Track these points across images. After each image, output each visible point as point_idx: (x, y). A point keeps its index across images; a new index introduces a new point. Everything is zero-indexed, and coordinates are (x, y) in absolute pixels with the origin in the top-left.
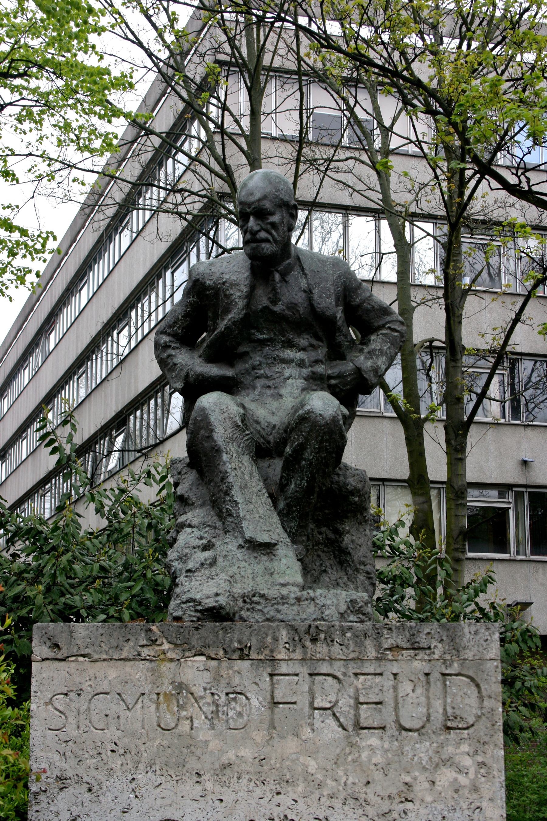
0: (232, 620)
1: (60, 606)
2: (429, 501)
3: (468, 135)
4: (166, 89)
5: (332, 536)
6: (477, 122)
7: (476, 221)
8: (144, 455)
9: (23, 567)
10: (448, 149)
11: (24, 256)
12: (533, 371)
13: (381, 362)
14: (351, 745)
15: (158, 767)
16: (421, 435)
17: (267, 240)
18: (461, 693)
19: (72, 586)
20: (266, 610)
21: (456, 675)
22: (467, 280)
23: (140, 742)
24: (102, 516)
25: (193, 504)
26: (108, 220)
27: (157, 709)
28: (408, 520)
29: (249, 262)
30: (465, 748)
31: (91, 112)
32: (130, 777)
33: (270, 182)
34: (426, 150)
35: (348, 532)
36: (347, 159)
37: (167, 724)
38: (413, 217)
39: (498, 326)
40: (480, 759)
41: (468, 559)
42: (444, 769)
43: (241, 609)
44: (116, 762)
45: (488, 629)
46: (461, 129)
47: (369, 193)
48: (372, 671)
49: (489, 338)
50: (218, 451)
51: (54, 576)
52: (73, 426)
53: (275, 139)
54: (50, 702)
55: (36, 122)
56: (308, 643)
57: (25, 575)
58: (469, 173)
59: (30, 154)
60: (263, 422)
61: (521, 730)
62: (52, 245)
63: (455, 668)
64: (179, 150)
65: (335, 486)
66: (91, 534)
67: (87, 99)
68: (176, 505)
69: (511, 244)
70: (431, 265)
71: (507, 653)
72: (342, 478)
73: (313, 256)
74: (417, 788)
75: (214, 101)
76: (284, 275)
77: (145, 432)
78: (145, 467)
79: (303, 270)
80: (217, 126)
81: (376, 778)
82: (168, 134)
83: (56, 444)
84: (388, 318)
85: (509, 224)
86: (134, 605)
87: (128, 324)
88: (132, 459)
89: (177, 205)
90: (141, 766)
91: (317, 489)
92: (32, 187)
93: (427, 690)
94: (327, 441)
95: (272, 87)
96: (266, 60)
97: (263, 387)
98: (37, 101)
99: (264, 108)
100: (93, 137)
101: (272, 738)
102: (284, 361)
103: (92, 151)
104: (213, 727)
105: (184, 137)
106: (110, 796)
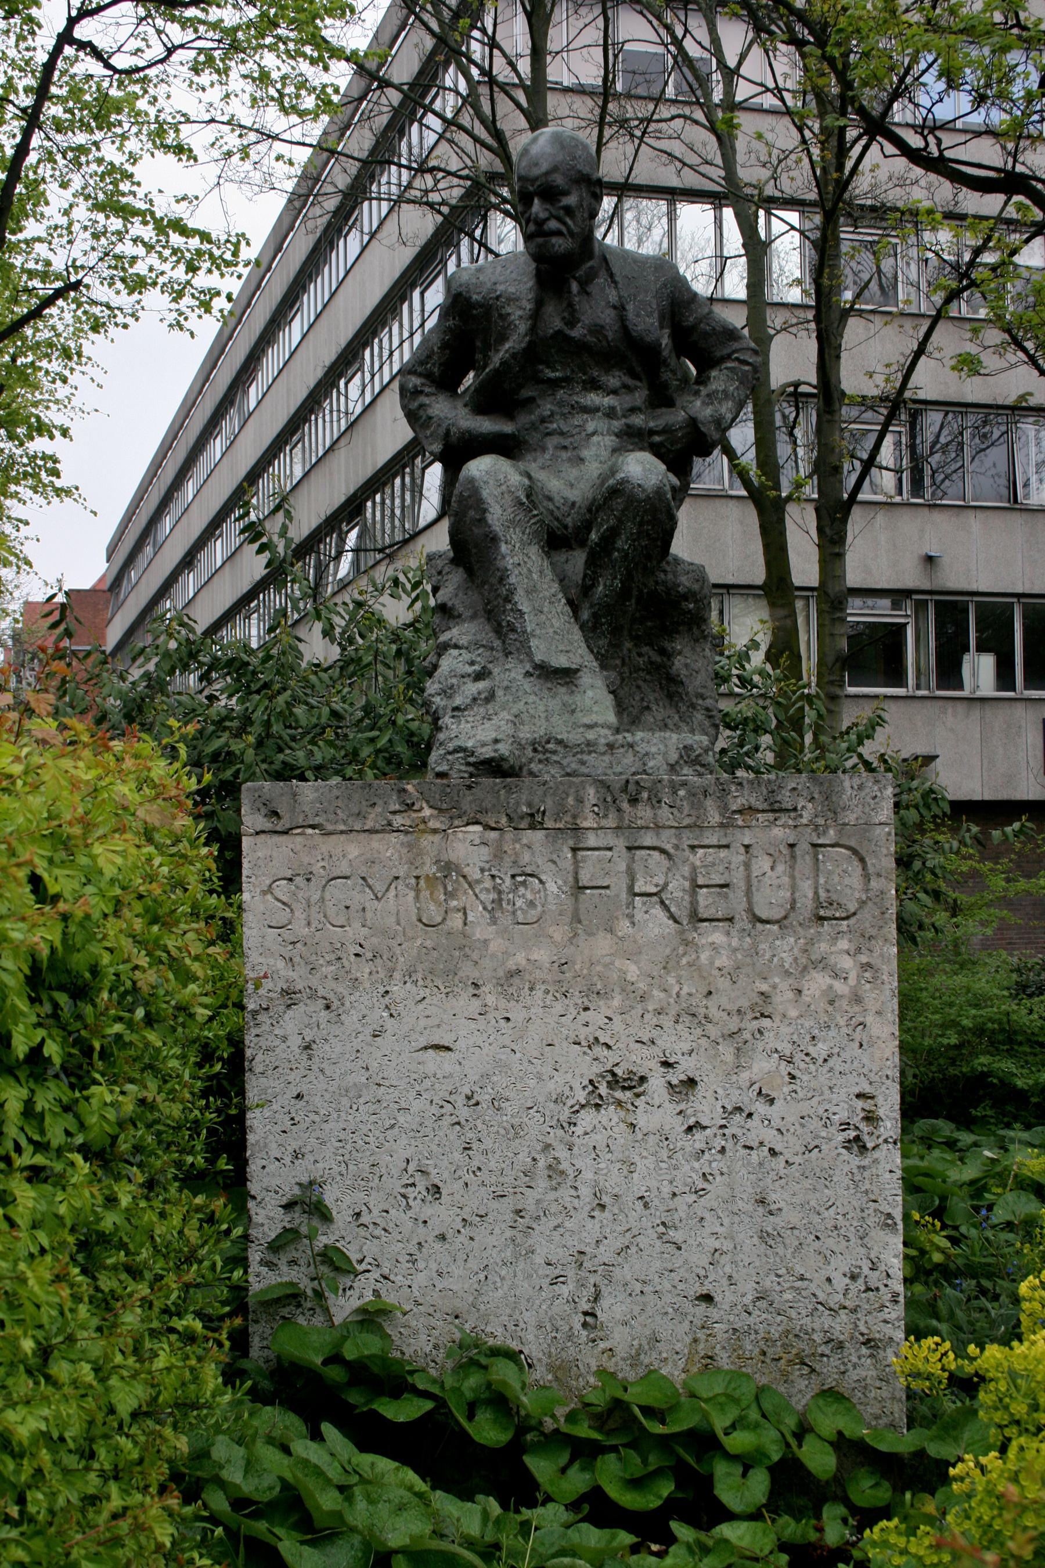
0: (518, 775)
1: (277, 766)
2: (793, 615)
3: (851, 75)
4: (407, 18)
5: (657, 658)
6: (866, 55)
7: (862, 207)
8: (389, 556)
9: (224, 712)
10: (820, 96)
11: (210, 271)
12: (942, 427)
13: (725, 409)
14: (687, 943)
15: (419, 976)
16: (782, 521)
17: (558, 233)
18: (839, 870)
19: (293, 739)
20: (565, 762)
21: (832, 846)
22: (848, 295)
23: (394, 943)
24: (332, 641)
25: (459, 616)
26: (328, 217)
27: (417, 898)
28: (764, 640)
29: (534, 265)
30: (843, 944)
32: (382, 990)
33: (563, 147)
34: (790, 102)
35: (680, 653)
36: (673, 118)
37: (431, 918)
38: (770, 203)
39: (893, 360)
40: (864, 959)
41: (848, 696)
42: (814, 974)
43: (531, 760)
44: (363, 970)
45: (877, 782)
46: (840, 66)
47: (705, 169)
48: (715, 842)
49: (880, 379)
50: (494, 540)
51: (267, 724)
52: (288, 515)
53: (567, 90)
55: (218, 72)
56: (625, 805)
57: (228, 724)
58: (851, 134)
59: (212, 121)
60: (557, 498)
61: (921, 927)
62: (248, 253)
64: (429, 109)
65: (659, 588)
66: (317, 665)
67: (292, 35)
68: (437, 619)
69: (912, 240)
70: (797, 274)
71: (902, 823)
72: (670, 576)
73: (626, 255)
74: (777, 999)
75: (476, 33)
77: (388, 526)
78: (390, 572)
79: (612, 275)
80: (483, 72)
81: (721, 986)
82: (412, 85)
83: (264, 540)
84: (736, 345)
85: (910, 211)
86: (379, 763)
87: (361, 368)
88: (371, 563)
89: (426, 192)
90: (397, 975)
91: (635, 593)
92: (214, 169)
93: (792, 867)
94: (649, 522)
97: (556, 448)
98: (220, 41)
99: (552, 45)
100: (303, 93)
101: (576, 935)
103: (302, 114)
104: (494, 921)
105: (434, 90)
106: (355, 1015)
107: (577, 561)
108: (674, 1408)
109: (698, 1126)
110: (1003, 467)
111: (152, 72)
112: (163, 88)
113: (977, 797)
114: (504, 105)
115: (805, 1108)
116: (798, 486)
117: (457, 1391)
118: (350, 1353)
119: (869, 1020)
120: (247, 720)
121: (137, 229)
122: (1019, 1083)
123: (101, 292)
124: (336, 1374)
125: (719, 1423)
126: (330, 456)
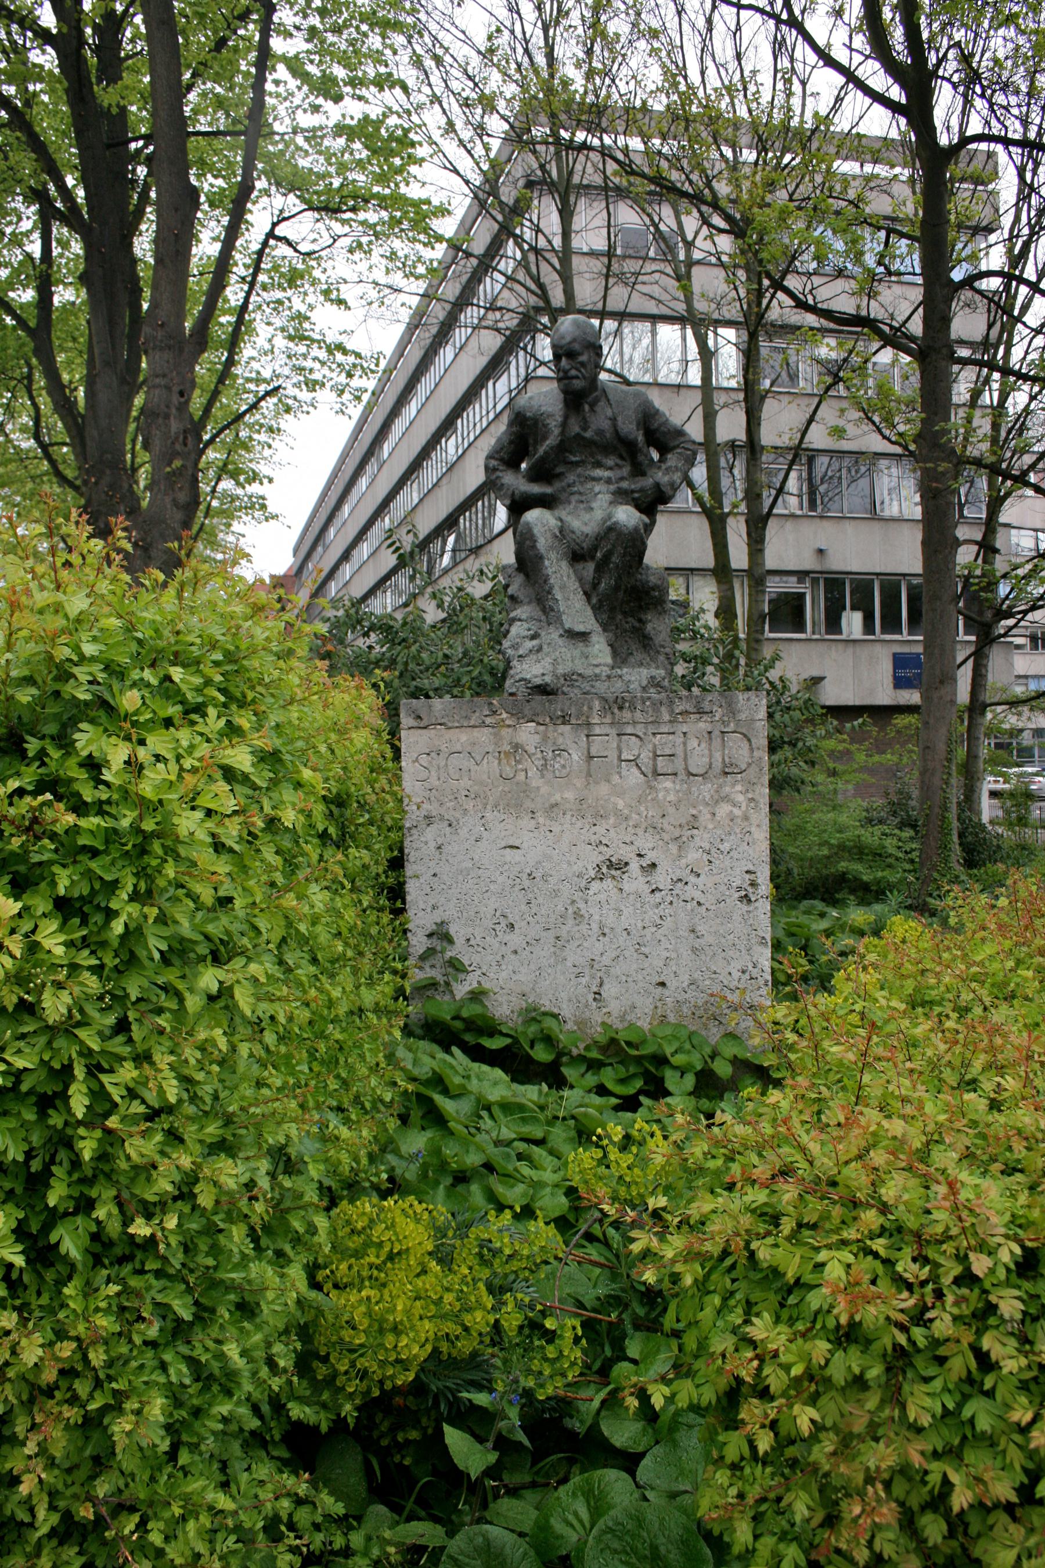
2: (732, 588)
16: (724, 529)
22: (767, 383)
30: (739, 788)
31: (414, 240)
38: (718, 323)
44: (469, 805)
50: (540, 558)
51: (406, 664)
54: (417, 760)
63: (732, 726)
74: (701, 819)
76: (592, 406)
92: (362, 311)
95: (582, 203)
96: (576, 179)
99: (575, 227)
102: (594, 479)
106: (465, 830)
107: (590, 567)
108: (644, 1042)
109: (657, 889)
110: (867, 492)
111: (323, 253)
112: (330, 263)
113: (851, 703)
114: (544, 267)
115: (717, 879)
116: (735, 506)
117: (524, 1033)
118: (465, 1014)
119: (753, 829)
120: (393, 662)
121: (315, 352)
122: (865, 878)
123: (291, 391)
124: (458, 1025)
125: (668, 1050)
126: (437, 489)
